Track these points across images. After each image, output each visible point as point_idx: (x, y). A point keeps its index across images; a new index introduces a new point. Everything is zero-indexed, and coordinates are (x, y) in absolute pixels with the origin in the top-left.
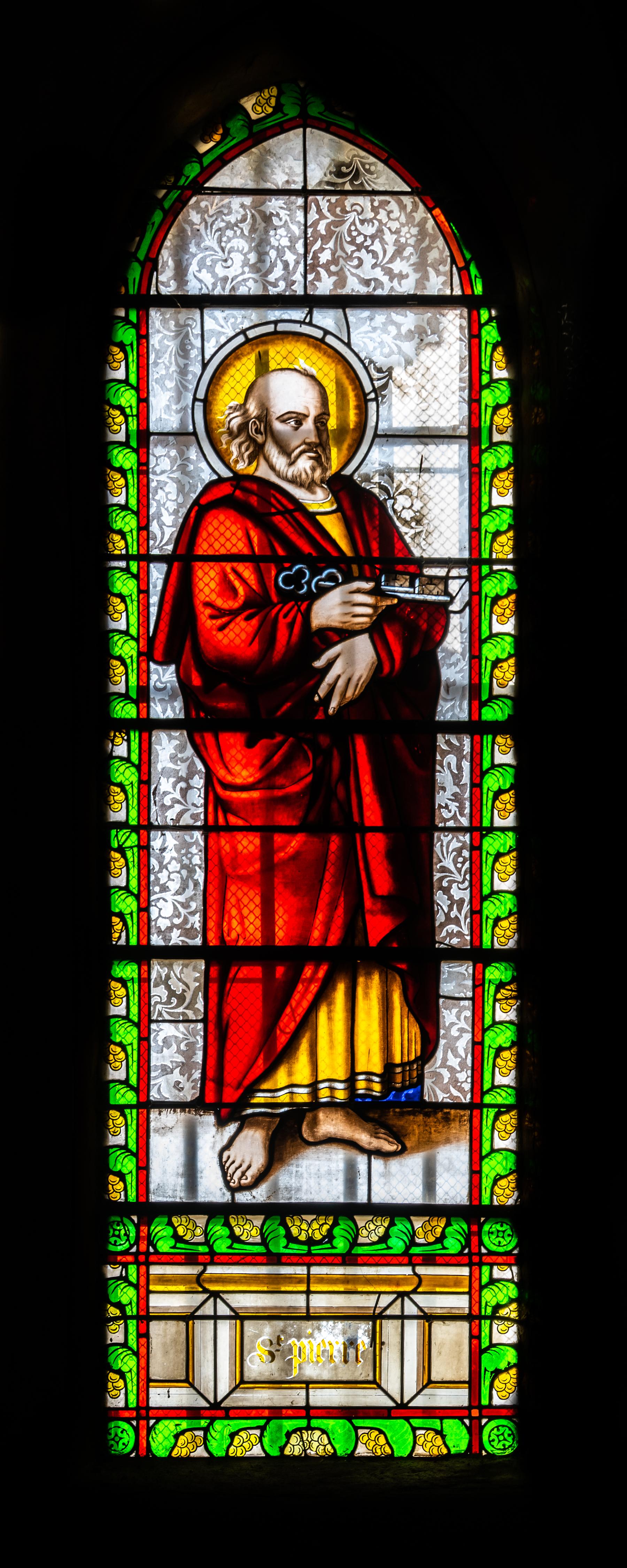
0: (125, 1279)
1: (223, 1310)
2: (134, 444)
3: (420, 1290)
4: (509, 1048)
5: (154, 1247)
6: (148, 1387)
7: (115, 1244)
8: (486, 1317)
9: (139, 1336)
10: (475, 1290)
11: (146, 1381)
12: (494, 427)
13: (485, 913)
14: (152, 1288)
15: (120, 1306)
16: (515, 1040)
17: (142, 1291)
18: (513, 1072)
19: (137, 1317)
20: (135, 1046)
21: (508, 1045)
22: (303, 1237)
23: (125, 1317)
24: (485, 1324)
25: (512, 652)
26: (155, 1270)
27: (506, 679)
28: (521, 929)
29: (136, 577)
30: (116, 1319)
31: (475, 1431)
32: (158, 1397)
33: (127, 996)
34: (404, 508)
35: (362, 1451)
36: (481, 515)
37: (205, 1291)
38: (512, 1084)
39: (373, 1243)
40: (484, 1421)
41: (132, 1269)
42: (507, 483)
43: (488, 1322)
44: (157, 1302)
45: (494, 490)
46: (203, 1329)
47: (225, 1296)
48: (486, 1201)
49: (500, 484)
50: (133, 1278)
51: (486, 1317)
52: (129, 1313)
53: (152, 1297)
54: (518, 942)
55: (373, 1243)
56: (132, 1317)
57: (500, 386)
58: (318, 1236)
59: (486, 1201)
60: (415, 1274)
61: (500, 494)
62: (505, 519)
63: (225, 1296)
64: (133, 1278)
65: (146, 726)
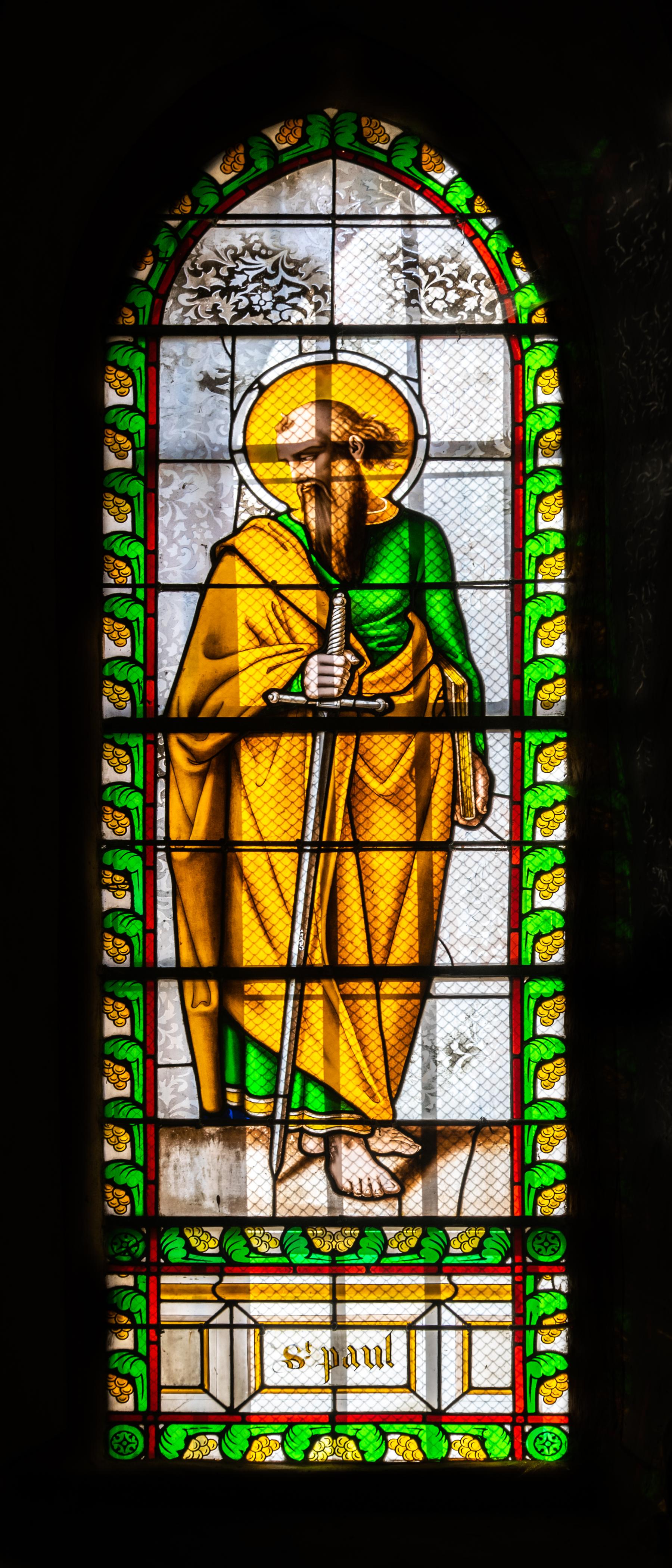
0: (135, 1288)
1: (240, 1318)
2: (141, 471)
3: (456, 1298)
4: (553, 429)
5: (165, 1257)
6: (159, 1393)
7: (117, 1451)
8: (530, 1327)
9: (149, 1343)
10: (519, 1299)
11: (155, 1389)
12: (539, 702)
13: (527, 363)
14: (163, 1297)
15: (129, 1314)
16: (558, 419)
17: (153, 1298)
18: (566, 1393)
19: (147, 1327)
20: (141, 1189)
21: (551, 426)
22: (325, 1249)
23: (135, 1326)
24: (530, 1334)
25: (560, 484)
26: (165, 1280)
27: (556, 1401)
28: (569, 945)
29: (143, 603)
30: (125, 1326)
31: (517, 1440)
32: (170, 1402)
33: (132, 1079)
34: (436, 299)
35: (391, 1456)
36: (524, 665)
37: (220, 1300)
38: (561, 1033)
39: (404, 1254)
40: (527, 1428)
41: (142, 1279)
42: (553, 381)
43: (532, 1332)
44: (169, 1311)
45: (539, 389)
46: (218, 1340)
47: (240, 1304)
48: (528, 1212)
49: (546, 509)
50: (142, 1287)
51: (530, 1327)
52: (138, 1321)
53: (163, 1306)
54: (566, 956)
55: (404, 1254)
56: (142, 1326)
57: (547, 1043)
58: (342, 1248)
59: (528, 1212)
60: (451, 1283)
61: (544, 392)
62: (550, 418)
63: (240, 1304)
64: (142, 1287)
65: (149, 974)
